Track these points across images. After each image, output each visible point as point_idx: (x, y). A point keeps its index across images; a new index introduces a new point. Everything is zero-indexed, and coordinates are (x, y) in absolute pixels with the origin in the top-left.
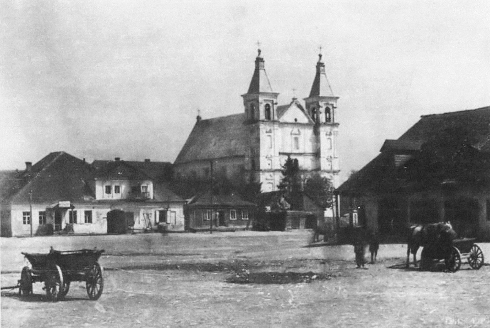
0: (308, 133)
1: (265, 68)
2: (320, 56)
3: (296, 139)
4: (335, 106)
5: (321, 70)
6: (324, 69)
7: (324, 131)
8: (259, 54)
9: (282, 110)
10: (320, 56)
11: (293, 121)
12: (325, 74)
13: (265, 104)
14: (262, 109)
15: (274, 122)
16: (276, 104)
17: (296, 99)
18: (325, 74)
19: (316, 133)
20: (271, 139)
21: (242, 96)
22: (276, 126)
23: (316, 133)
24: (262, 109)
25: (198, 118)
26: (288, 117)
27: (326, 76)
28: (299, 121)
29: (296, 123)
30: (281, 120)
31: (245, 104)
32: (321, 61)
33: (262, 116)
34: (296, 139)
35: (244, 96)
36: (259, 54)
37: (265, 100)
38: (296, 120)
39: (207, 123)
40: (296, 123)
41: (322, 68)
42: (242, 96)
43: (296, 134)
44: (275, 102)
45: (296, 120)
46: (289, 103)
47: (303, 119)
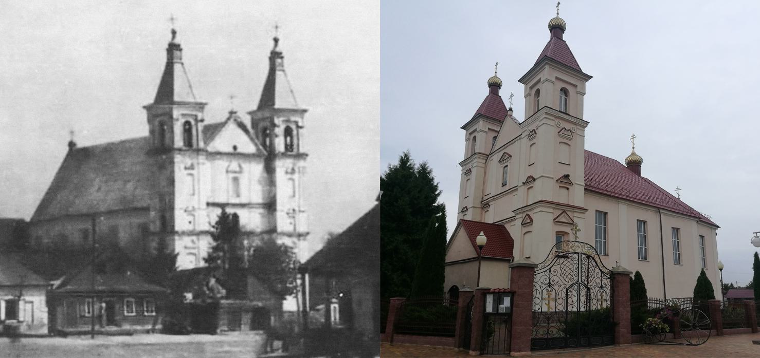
0: (256, 169)
1: (183, 61)
2: (276, 40)
3: (236, 180)
4: (300, 124)
5: (277, 64)
6: (283, 62)
7: (282, 166)
8: (174, 37)
9: (212, 130)
10: (276, 40)
11: (231, 150)
12: (283, 71)
13: (183, 120)
14: (178, 129)
15: (198, 151)
16: (202, 121)
17: (235, 113)
18: (283, 71)
19: (270, 170)
20: (193, 180)
21: (144, 107)
22: (202, 158)
23: (270, 170)
24: (178, 129)
25: (71, 144)
26: (221, 143)
27: (285, 75)
28: (239, 150)
29: (235, 154)
30: (210, 148)
31: (150, 121)
32: (278, 50)
33: (179, 142)
34: (236, 180)
35: (148, 108)
36: (174, 37)
37: (183, 115)
38: (235, 148)
39: (87, 153)
40: (235, 154)
41: (279, 61)
42: (144, 107)
43: (235, 172)
44: (199, 118)
45: (235, 148)
46: (224, 120)
47: (247, 146)
